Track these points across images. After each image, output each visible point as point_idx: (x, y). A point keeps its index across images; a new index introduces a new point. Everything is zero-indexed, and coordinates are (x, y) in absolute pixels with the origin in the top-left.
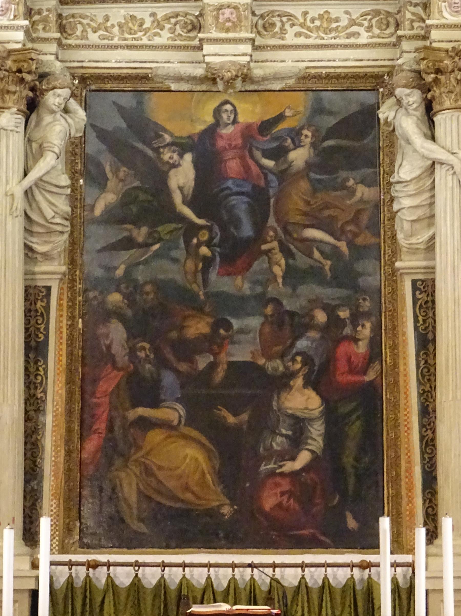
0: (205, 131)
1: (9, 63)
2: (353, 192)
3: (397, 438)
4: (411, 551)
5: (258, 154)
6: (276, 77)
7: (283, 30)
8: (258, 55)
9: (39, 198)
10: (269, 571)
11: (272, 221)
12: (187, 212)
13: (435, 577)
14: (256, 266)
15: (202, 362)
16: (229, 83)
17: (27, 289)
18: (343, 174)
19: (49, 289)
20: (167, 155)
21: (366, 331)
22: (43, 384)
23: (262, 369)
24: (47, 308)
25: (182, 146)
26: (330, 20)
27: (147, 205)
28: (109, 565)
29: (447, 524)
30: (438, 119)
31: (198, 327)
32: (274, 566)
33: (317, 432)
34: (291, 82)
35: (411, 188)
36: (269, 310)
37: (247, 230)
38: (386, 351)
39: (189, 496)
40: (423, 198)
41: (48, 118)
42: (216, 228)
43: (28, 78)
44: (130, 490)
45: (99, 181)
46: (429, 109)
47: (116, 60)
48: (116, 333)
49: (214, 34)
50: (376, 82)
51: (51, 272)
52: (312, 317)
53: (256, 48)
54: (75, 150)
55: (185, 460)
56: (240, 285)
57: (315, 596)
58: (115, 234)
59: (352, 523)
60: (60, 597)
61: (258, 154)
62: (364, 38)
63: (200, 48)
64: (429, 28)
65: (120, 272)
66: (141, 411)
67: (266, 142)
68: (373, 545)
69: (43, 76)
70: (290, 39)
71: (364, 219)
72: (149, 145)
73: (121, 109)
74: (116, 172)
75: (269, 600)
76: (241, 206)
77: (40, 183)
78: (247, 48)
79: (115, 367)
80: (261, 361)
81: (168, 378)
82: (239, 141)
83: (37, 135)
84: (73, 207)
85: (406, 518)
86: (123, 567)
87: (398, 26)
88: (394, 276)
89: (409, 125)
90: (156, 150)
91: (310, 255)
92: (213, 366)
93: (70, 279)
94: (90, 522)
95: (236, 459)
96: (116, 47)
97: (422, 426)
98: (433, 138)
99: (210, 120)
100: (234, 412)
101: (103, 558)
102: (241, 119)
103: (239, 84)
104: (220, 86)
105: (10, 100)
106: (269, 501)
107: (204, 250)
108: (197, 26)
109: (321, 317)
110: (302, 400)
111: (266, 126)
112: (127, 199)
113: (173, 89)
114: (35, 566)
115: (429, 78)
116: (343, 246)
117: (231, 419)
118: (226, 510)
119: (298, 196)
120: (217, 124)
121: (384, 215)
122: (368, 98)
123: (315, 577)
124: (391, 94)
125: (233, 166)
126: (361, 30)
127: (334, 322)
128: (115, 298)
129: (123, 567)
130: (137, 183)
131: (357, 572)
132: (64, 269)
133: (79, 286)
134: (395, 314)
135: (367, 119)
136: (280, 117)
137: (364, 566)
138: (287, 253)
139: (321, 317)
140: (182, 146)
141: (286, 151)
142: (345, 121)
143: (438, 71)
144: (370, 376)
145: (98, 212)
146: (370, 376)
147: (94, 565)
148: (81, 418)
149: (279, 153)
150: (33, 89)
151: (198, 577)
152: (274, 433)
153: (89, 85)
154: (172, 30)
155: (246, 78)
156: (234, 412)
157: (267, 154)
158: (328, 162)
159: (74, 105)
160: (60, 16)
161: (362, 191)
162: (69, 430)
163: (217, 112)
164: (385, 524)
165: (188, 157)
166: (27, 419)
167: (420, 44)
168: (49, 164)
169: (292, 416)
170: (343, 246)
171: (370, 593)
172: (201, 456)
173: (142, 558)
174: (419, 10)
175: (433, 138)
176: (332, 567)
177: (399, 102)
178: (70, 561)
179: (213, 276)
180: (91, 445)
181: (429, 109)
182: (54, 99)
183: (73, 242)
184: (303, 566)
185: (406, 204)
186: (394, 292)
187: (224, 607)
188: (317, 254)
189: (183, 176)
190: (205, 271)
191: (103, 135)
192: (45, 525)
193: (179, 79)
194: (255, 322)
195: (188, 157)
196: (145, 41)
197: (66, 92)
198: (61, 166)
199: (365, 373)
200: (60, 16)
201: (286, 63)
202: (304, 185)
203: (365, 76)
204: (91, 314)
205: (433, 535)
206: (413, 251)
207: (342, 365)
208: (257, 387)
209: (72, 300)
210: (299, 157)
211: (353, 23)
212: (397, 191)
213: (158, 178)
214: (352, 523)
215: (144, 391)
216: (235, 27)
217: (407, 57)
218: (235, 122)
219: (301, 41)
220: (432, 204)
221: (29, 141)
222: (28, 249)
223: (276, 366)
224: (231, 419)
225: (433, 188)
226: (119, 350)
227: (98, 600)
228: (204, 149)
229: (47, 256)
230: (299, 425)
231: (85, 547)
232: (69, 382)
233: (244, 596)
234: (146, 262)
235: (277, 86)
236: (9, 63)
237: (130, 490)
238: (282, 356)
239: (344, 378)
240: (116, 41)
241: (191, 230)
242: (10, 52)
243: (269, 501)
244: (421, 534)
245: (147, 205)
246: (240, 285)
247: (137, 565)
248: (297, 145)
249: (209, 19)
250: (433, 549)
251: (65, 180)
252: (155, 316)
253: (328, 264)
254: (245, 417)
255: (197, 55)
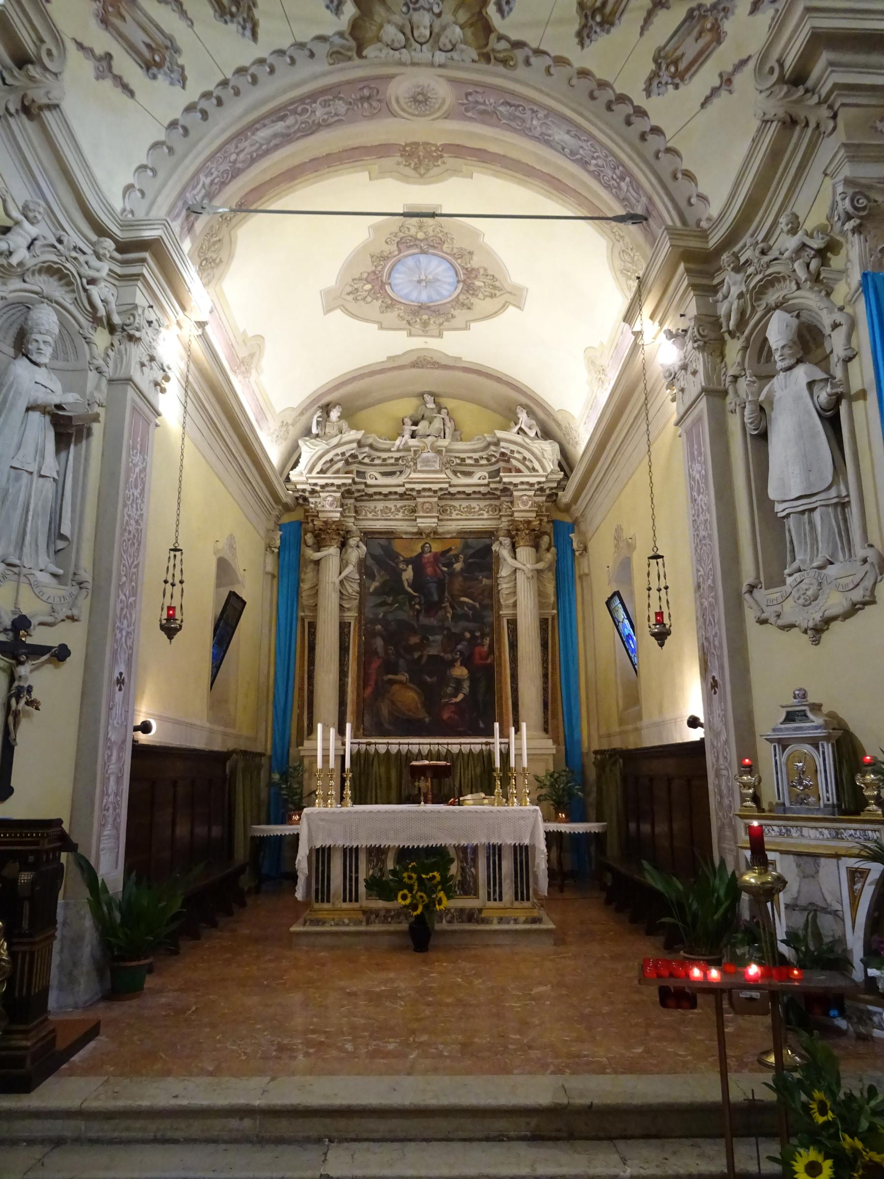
0: (417, 556)
1: (334, 526)
2: (482, 582)
3: (501, 687)
4: (508, 737)
5: (440, 565)
6: (448, 532)
7: (451, 513)
8: (440, 523)
9: (345, 583)
10: (446, 746)
11: (446, 594)
12: (410, 590)
13: (519, 748)
14: (440, 613)
15: (416, 655)
16: (428, 535)
17: (341, 623)
18: (477, 574)
19: (350, 623)
20: (401, 566)
21: (487, 641)
22: (348, 665)
23: (442, 658)
24: (349, 632)
25: (407, 562)
26: (471, 508)
27: (392, 587)
28: (376, 744)
29: (524, 726)
30: (517, 550)
31: (414, 640)
32: (448, 744)
33: (466, 685)
34: (454, 535)
35: (506, 580)
36: (445, 632)
37: (436, 597)
38: (496, 651)
39: (411, 713)
40: (511, 584)
41: (350, 550)
42: (422, 597)
43: (342, 533)
44: (385, 711)
45: (372, 577)
46: (514, 547)
47: (379, 525)
48: (379, 643)
49: (422, 514)
50: (491, 535)
51: (351, 616)
52: (464, 636)
53: (439, 520)
54: (362, 565)
55: (409, 698)
56: (432, 621)
57: (466, 758)
58: (379, 600)
59: (482, 725)
60: (354, 758)
61: (440, 565)
62: (486, 516)
63: (415, 520)
64: (513, 512)
65: (381, 616)
66: (390, 676)
67: (443, 560)
68: (491, 734)
69: (348, 532)
70: (454, 516)
71: (486, 594)
72: (393, 561)
73: (382, 547)
74: (379, 572)
75: (445, 759)
76: (433, 587)
77: (346, 578)
78: (436, 520)
79: (379, 657)
80: (442, 654)
81: (401, 662)
82: (432, 560)
83: (345, 557)
84: (360, 587)
85: (505, 723)
86: (382, 745)
87: (500, 511)
88: (499, 617)
89: (505, 553)
90: (397, 564)
91: (463, 609)
92: (420, 657)
93: (359, 619)
94: (367, 724)
95: (431, 697)
96: (379, 520)
97: (512, 683)
98: (515, 558)
99: (420, 550)
100: (430, 677)
101: (373, 741)
102: (433, 550)
103: (432, 535)
104: (424, 536)
105: (334, 542)
106: (445, 716)
107: (417, 607)
108: (414, 511)
109: (468, 635)
110: (460, 671)
111: (444, 553)
112: (384, 584)
113: (777, 854)
114: (344, 744)
115: (514, 533)
116: (477, 605)
117: (429, 679)
118: (427, 720)
119: (458, 582)
120: (423, 552)
121: (495, 592)
122: (488, 541)
123: (466, 749)
124: (498, 540)
125: (429, 570)
126: (484, 513)
127: (473, 637)
128: (379, 627)
129: (382, 745)
130: (388, 578)
131: (484, 747)
132: (357, 615)
133: (363, 622)
134: (500, 635)
135: (487, 551)
136: (450, 550)
137: (487, 744)
138: (453, 607)
139: (468, 635)
140: (407, 562)
141: (453, 564)
142: (478, 551)
143: (517, 530)
144: (489, 661)
145: (371, 590)
146: (489, 661)
147: (369, 744)
148: (363, 680)
149: (449, 565)
150: (343, 538)
151: (415, 749)
152: (448, 686)
153: (368, 536)
154: (403, 513)
155: (435, 533)
156: (430, 677)
157: (444, 565)
158: (469, 568)
159: (361, 544)
160: (355, 507)
161: (485, 581)
162: (358, 685)
163: (423, 547)
164: (497, 725)
165: (410, 567)
166: (340, 680)
167: (510, 518)
168: (350, 569)
169: (456, 679)
170: (477, 605)
171: (490, 754)
172: (416, 696)
173: (390, 741)
174: (509, 504)
175: (515, 558)
176: (473, 744)
177: (501, 543)
178: (241, 1119)
179: (421, 618)
180: (369, 690)
181: (514, 547)
182: (353, 542)
183: (360, 603)
184: (460, 744)
185: (504, 587)
186: (499, 624)
187: (426, 762)
188: (466, 608)
189: (408, 574)
190: (418, 616)
191: (374, 557)
192: (348, 726)
193: (406, 533)
194: (439, 638)
195: (410, 567)
196: (392, 517)
197: (358, 539)
198: (356, 570)
199: (487, 659)
200: (355, 507)
201: (452, 526)
202: (460, 579)
203: (486, 532)
204: (368, 634)
205: (517, 730)
206: (507, 607)
207: (477, 657)
208: (441, 665)
209: (360, 628)
210: (458, 566)
211: (481, 509)
212: (500, 581)
213: (397, 574)
214: (482, 725)
215: (390, 667)
216: (431, 511)
217: (504, 524)
218: (430, 551)
219: (459, 517)
220: (515, 587)
221: (342, 560)
222: (341, 606)
223: (449, 656)
224: (429, 679)
225: (515, 579)
226: (380, 650)
227: (371, 759)
228: (417, 562)
229: (349, 609)
230: (459, 682)
231: (365, 736)
232: (358, 664)
233: (435, 758)
234: (391, 612)
235: (449, 536)
236: (334, 526)
237: (385, 711)
238: (451, 652)
239: (477, 660)
240: (379, 517)
241: (412, 598)
242: (334, 522)
243: (445, 716)
244: (513, 729)
245: (392, 587)
246: (432, 621)
247: (388, 743)
248: (457, 561)
249: (419, 507)
250: (517, 736)
251: (357, 576)
252: (395, 635)
253: (471, 612)
254: (435, 679)
255: (414, 523)
